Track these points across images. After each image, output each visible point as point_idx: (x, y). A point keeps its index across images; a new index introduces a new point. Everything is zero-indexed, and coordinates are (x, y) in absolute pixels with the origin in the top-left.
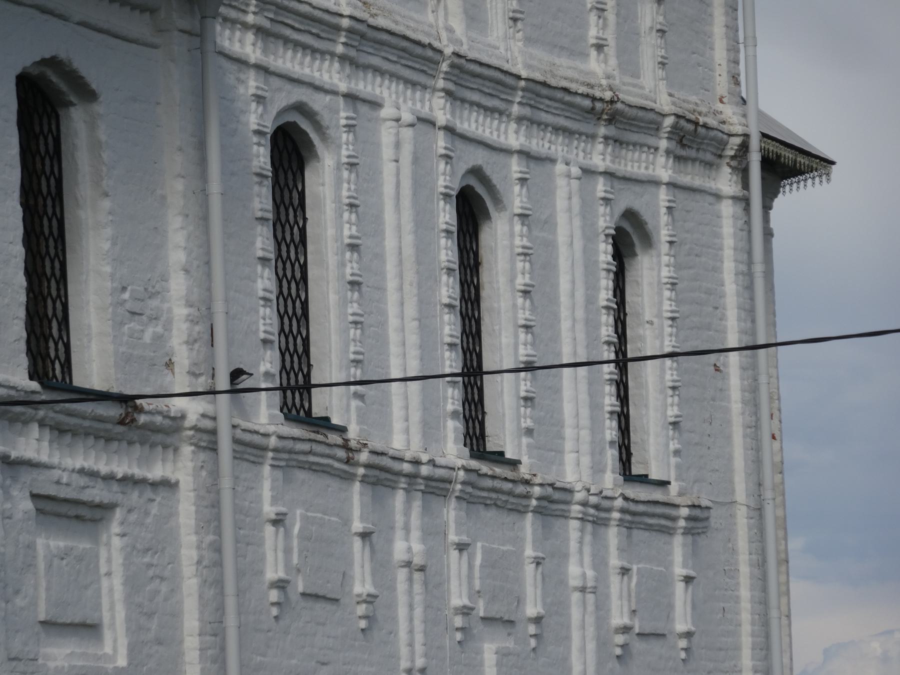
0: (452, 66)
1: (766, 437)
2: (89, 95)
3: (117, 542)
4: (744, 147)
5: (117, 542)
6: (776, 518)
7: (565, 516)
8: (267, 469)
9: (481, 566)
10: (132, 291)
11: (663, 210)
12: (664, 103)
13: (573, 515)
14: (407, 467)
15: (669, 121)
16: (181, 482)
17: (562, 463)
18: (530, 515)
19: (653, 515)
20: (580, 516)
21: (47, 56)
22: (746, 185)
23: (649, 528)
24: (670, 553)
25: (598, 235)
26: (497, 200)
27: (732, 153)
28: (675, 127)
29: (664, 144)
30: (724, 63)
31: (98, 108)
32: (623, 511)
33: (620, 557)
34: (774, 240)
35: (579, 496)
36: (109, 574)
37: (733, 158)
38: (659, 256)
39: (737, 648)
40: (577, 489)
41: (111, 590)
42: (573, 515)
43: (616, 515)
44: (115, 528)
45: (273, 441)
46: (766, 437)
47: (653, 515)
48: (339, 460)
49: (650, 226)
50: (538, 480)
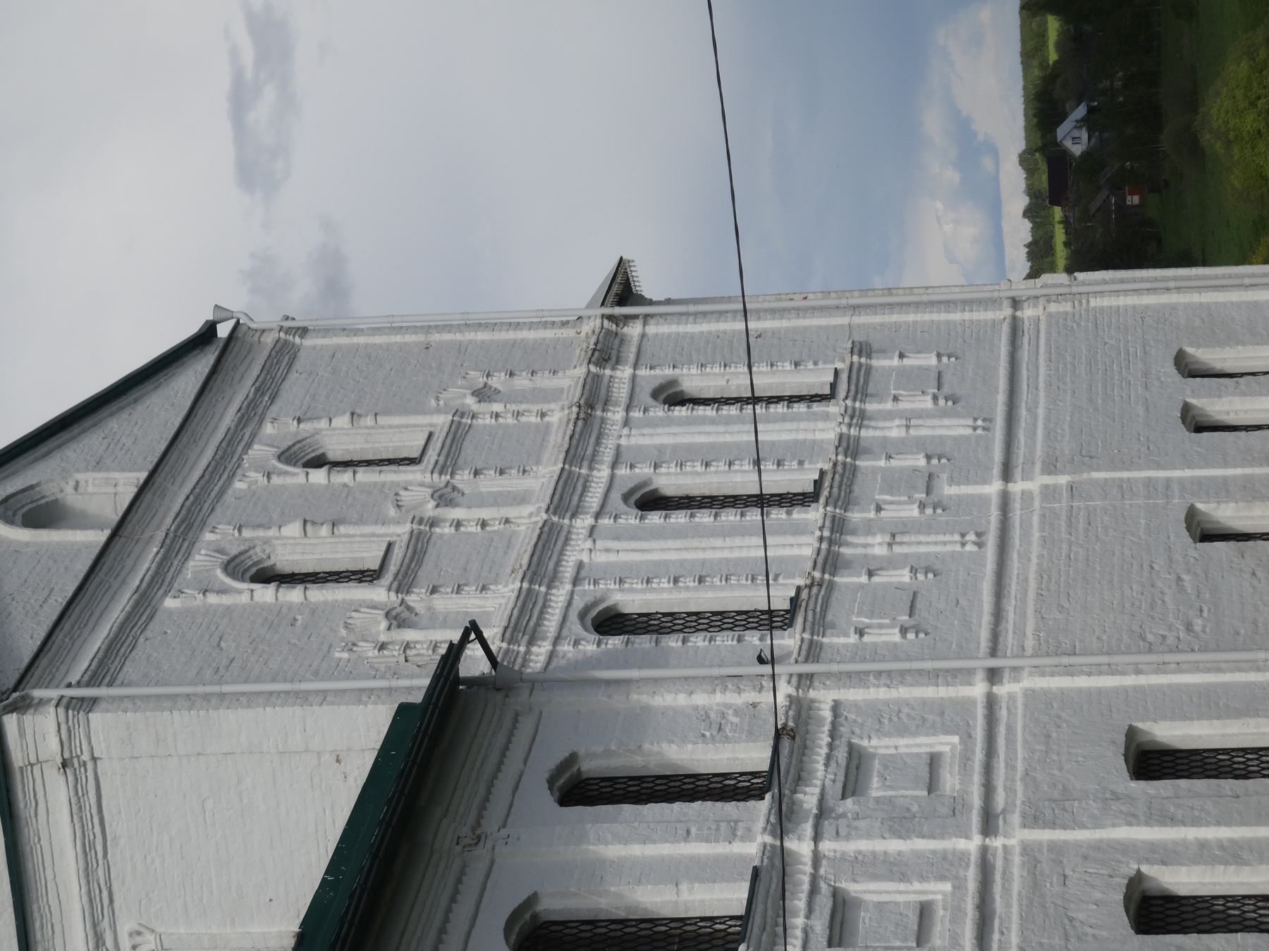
0: (555, 514)
3: (874, 742)
4: (610, 318)
7: (858, 439)
12: (581, 371)
13: (857, 433)
14: (824, 546)
15: (593, 369)
18: (857, 463)
19: (858, 379)
20: (858, 429)
21: (547, 785)
26: (645, 484)
27: (614, 326)
30: (554, 331)
31: (582, 752)
32: (855, 400)
34: (673, 297)
42: (857, 433)
43: (857, 404)
45: (807, 636)
47: (858, 379)
48: (819, 591)
50: (833, 457)
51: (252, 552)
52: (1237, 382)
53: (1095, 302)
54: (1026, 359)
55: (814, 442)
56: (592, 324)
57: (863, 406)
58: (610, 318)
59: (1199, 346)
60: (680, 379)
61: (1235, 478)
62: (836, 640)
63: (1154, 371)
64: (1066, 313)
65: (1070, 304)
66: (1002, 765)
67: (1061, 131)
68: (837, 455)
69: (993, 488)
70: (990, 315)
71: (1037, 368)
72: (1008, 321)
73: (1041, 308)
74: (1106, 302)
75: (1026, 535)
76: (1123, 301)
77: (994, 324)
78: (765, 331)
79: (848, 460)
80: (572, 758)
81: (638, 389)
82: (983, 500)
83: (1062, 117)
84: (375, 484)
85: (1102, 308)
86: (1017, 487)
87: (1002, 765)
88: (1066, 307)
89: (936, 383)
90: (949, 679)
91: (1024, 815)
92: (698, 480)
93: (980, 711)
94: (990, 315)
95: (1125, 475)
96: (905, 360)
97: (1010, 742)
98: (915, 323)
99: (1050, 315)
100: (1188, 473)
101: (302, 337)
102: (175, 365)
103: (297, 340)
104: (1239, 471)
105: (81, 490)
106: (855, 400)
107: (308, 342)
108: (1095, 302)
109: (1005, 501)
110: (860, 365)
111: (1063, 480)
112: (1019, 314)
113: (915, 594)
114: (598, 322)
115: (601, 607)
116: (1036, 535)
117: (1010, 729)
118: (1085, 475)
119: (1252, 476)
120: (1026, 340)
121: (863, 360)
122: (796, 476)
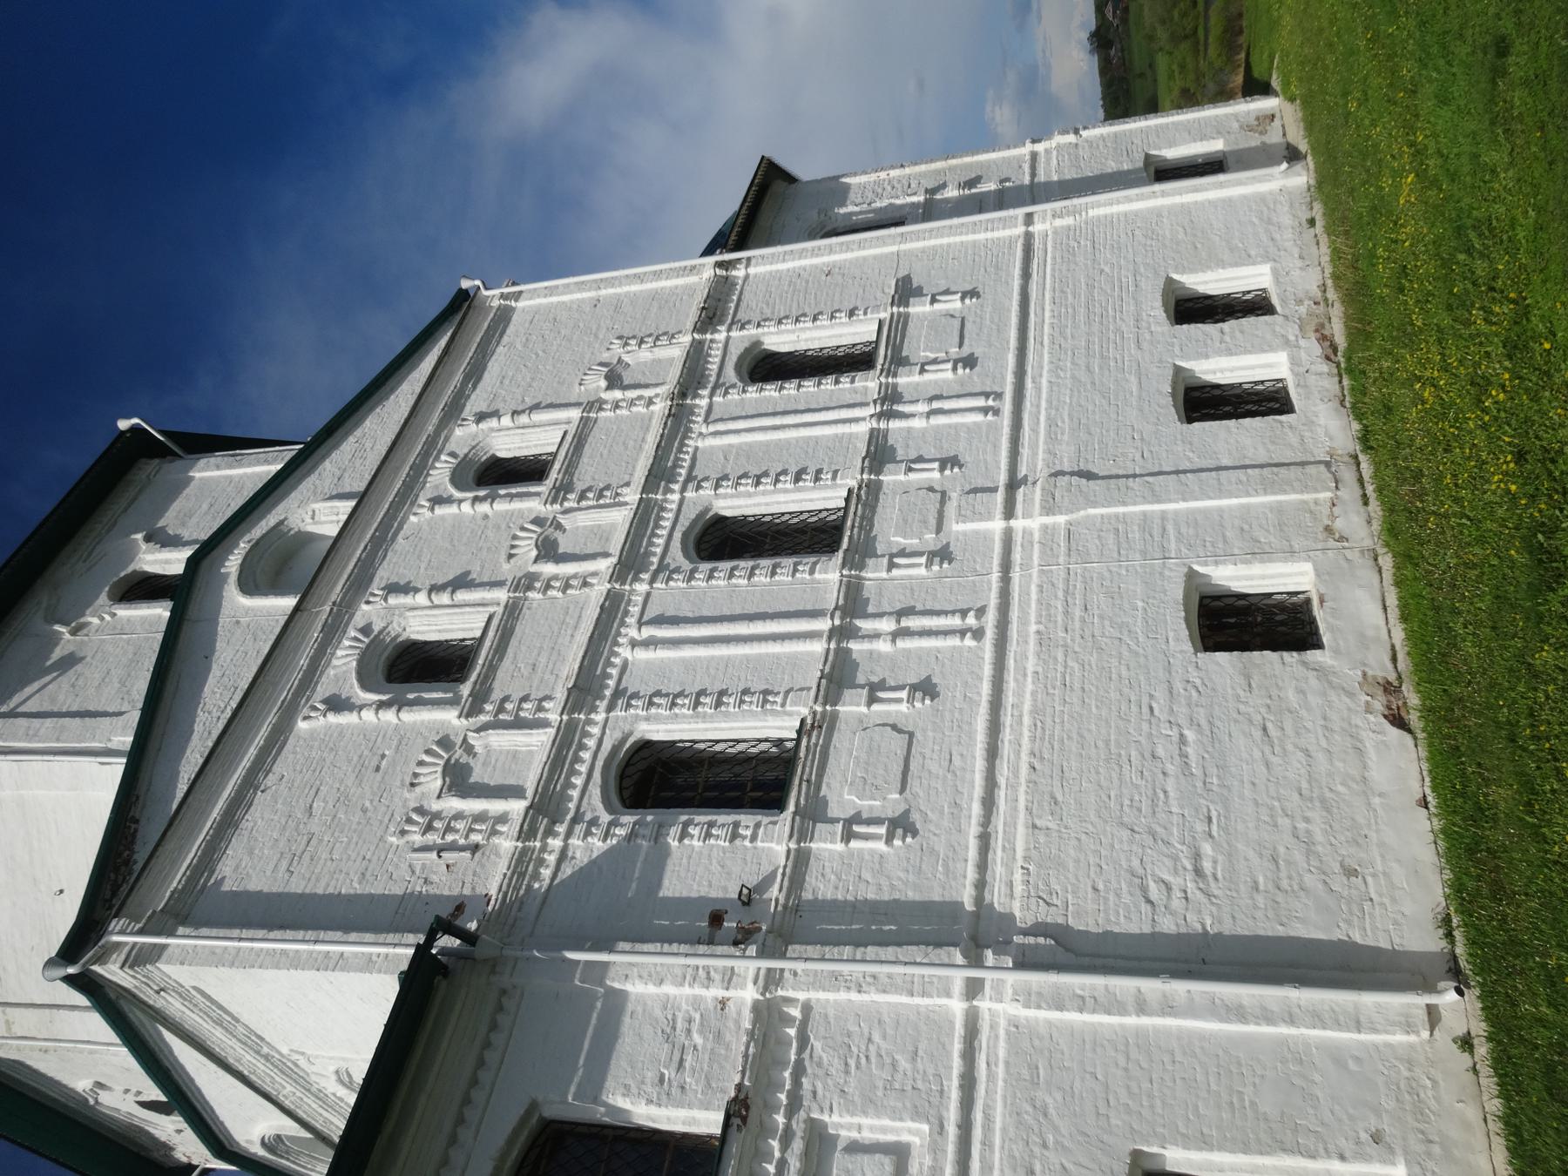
0: (616, 581)
2: (533, 1106)
3: (835, 1118)
4: (719, 265)
5: (835, 1118)
7: (895, 386)
8: (813, 845)
9: (904, 538)
10: (665, 1067)
11: (745, 332)
12: (686, 339)
15: (696, 336)
22: (739, 260)
23: (902, 341)
24: (917, 314)
26: (707, 510)
28: (529, 847)
29: (627, 587)
31: (540, 1099)
32: (887, 377)
36: (860, 1128)
38: (764, 334)
39: (974, 243)
41: (872, 1129)
43: (890, 380)
44: (825, 1118)
45: (793, 846)
48: (820, 734)
49: (747, 344)
51: (390, 628)
52: (1222, 332)
53: (1091, 213)
55: (851, 434)
58: (719, 265)
59: (1182, 273)
60: (762, 339)
61: (1230, 508)
62: (822, 845)
63: (1145, 317)
64: (1069, 228)
65: (1072, 218)
66: (1012, 662)
69: (997, 525)
70: (1007, 233)
71: (1043, 309)
73: (1048, 223)
78: (834, 264)
80: (533, 1106)
82: (986, 537)
84: (507, 511)
85: (1099, 218)
86: (1018, 524)
87: (1012, 662)
89: (957, 339)
91: (1043, 507)
93: (959, 1030)
94: (1007, 233)
95: (1121, 510)
97: (987, 1144)
98: (949, 245)
100: (1182, 505)
101: (516, 301)
102: (243, 525)
103: (513, 304)
104: (1234, 501)
105: (316, 518)
106: (887, 377)
107: (521, 304)
109: (1008, 538)
111: (1061, 519)
114: (712, 271)
115: (628, 745)
117: (988, 1119)
118: (1082, 513)
119: (1247, 507)
120: (1035, 261)
122: (829, 493)
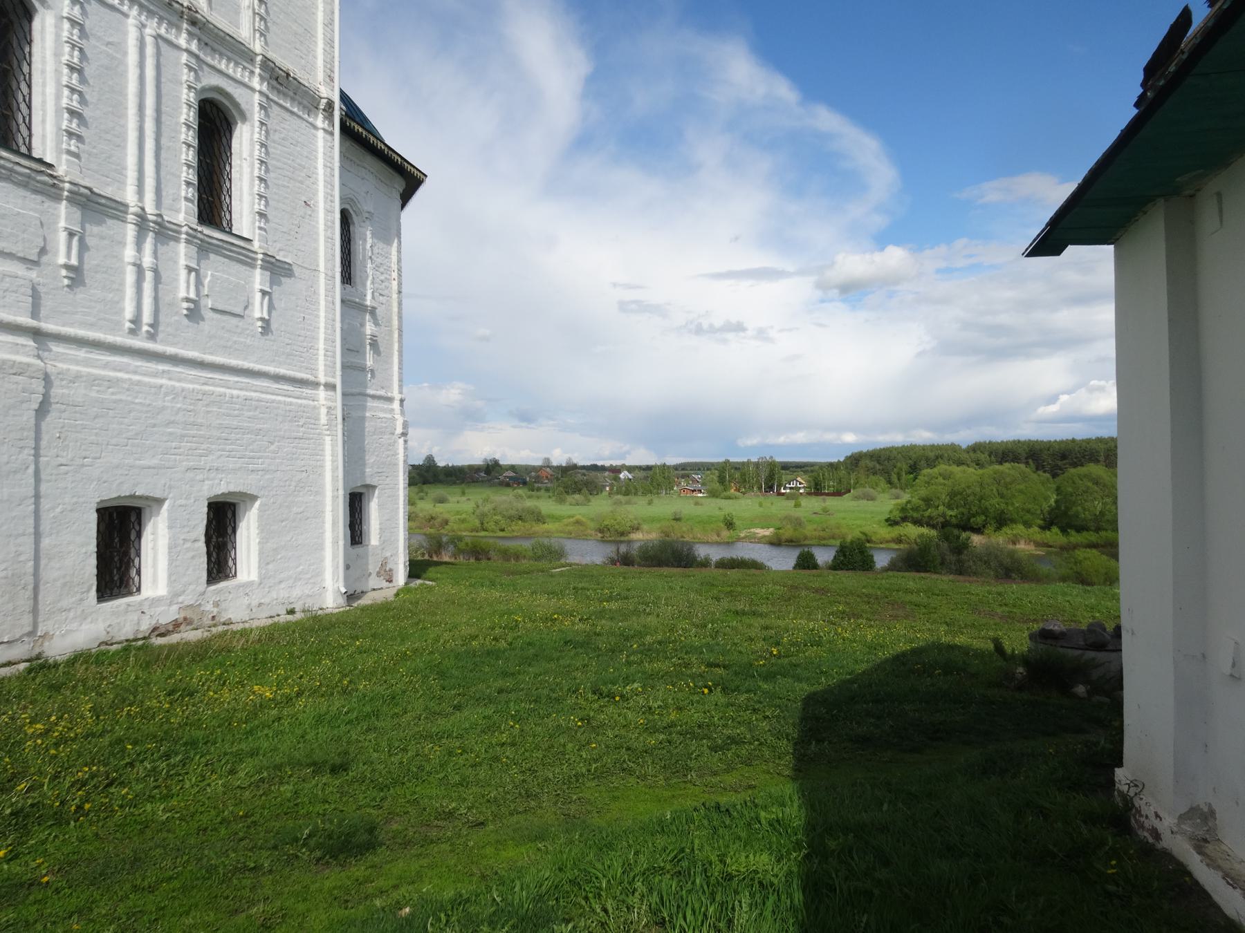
1: (501, 534)
6: (326, 220)
11: (257, 108)
13: (129, 221)
16: (93, 593)
17: (124, 190)
18: (64, 202)
19: (225, 249)
20: (135, 222)
25: (182, 84)
27: (323, 107)
30: (322, 67)
32: (187, 234)
33: (186, 260)
35: (131, 210)
37: (324, 110)
40: (131, 205)
42: (129, 221)
43: (184, 236)
46: (501, 534)
47: (225, 249)
50: (67, 179)
53: (328, 439)
54: (255, 383)
56: (325, 92)
57: (259, 266)
67: (626, 472)
68: (70, 183)
70: (321, 367)
72: (316, 380)
73: (324, 403)
74: (328, 448)
75: (86, 363)
76: (328, 458)
77: (313, 370)
79: (66, 193)
81: (301, 120)
83: (630, 472)
88: (323, 419)
90: (912, 531)
92: (49, 54)
94: (321, 367)
96: (260, 294)
99: (319, 408)
108: (328, 439)
110: (179, 232)
112: (322, 387)
113: (242, 317)
116: (85, 370)
120: (291, 388)
121: (259, 262)
